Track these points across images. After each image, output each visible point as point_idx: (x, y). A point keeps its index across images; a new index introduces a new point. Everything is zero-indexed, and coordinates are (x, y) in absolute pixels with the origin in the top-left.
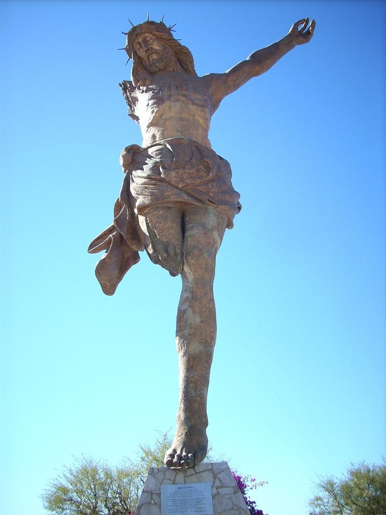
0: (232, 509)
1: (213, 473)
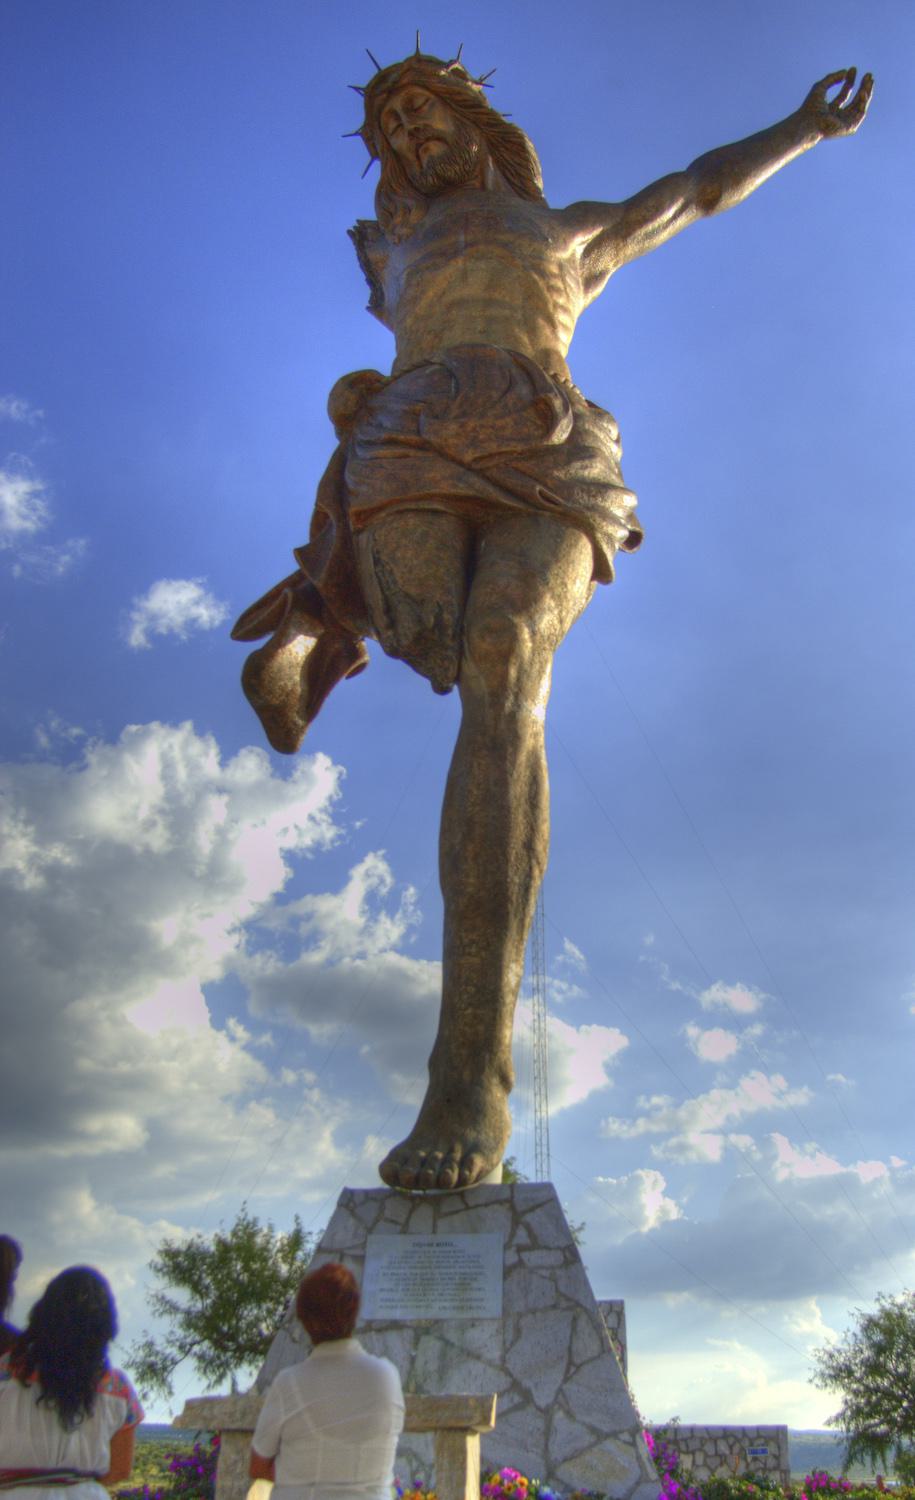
0: (554, 1307)
1: (513, 1208)
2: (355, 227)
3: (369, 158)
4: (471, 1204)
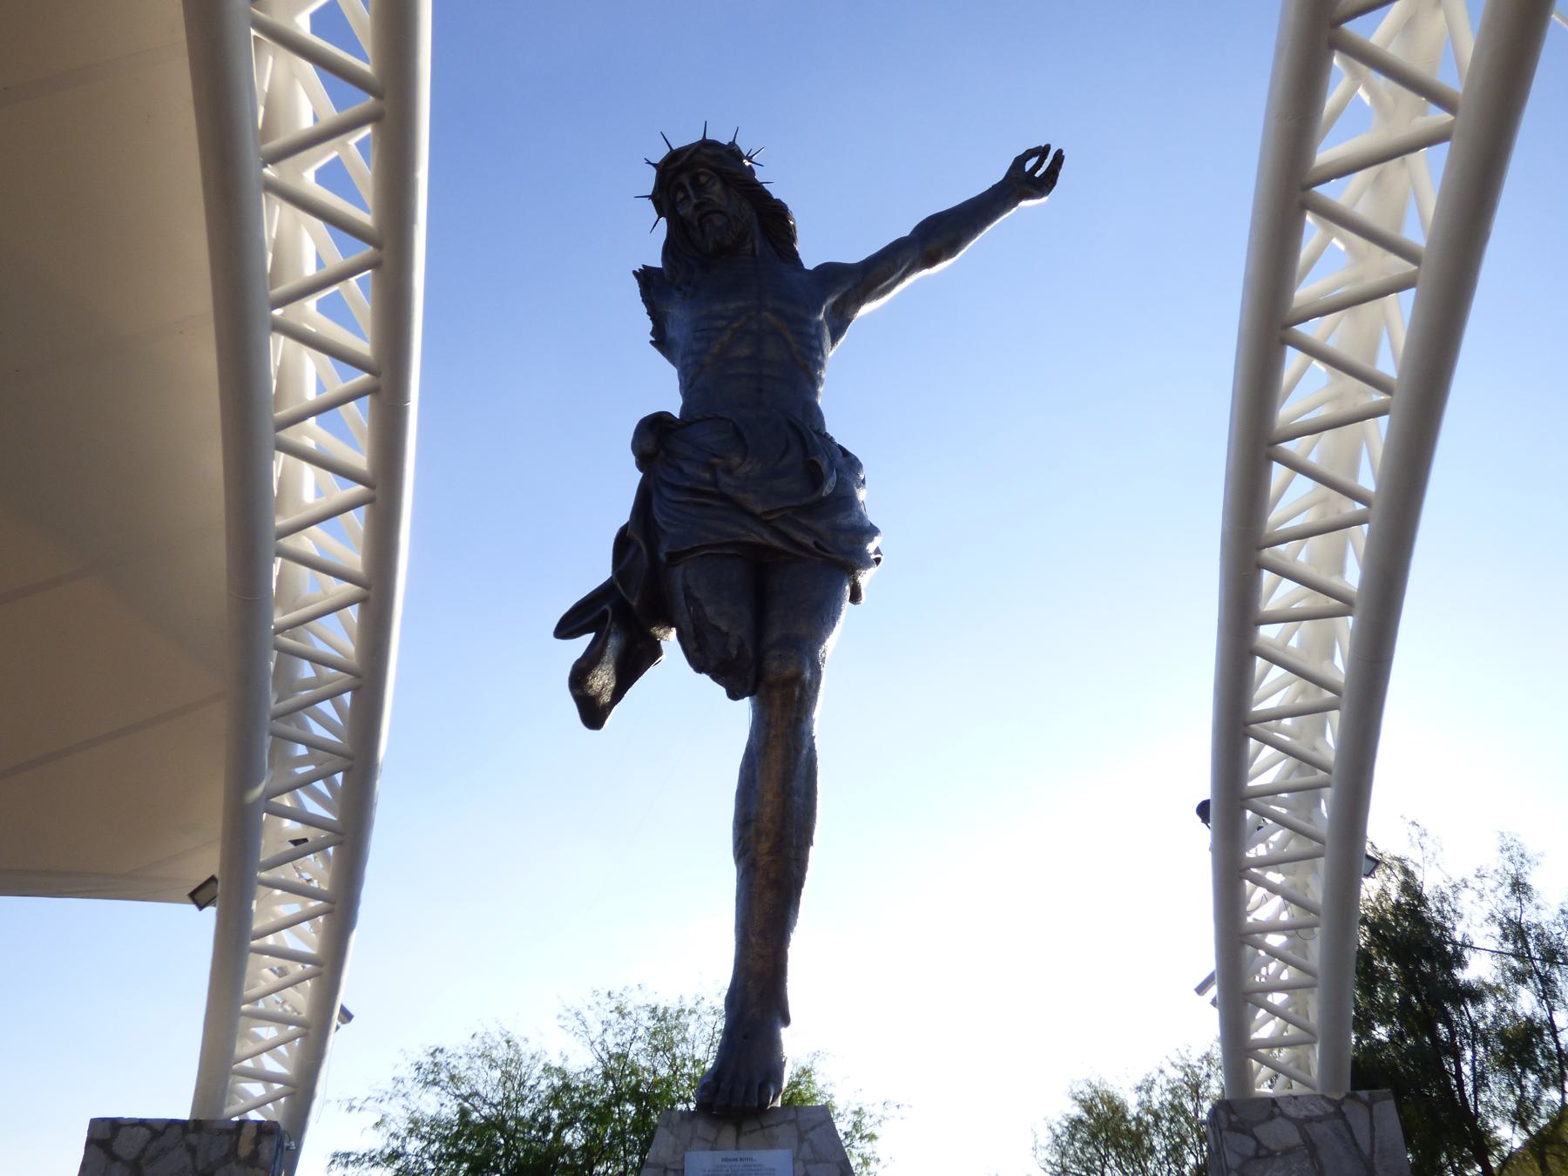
2: (640, 270)
3: (657, 216)
4: (765, 1125)
